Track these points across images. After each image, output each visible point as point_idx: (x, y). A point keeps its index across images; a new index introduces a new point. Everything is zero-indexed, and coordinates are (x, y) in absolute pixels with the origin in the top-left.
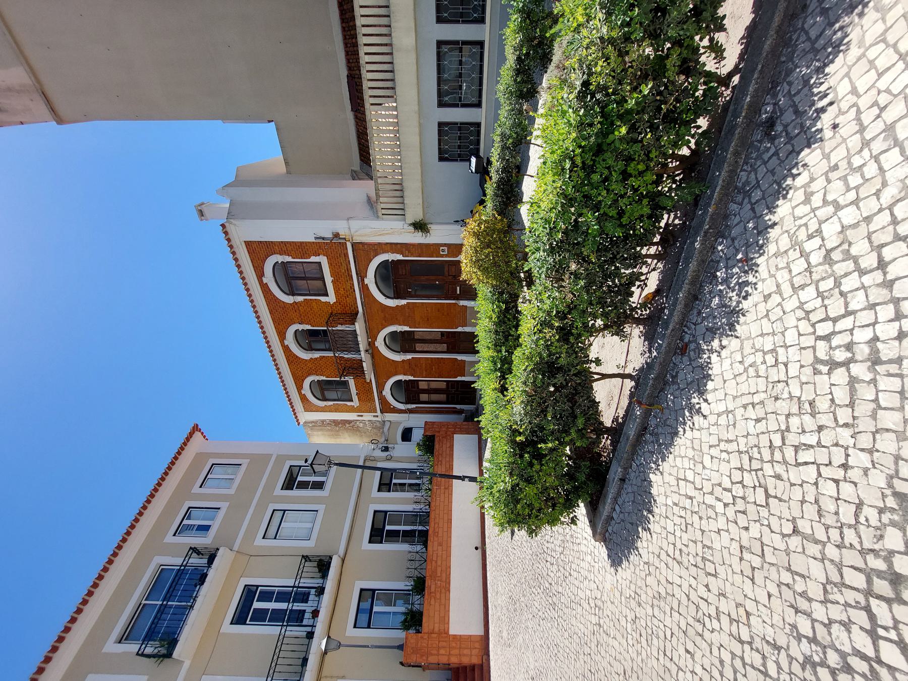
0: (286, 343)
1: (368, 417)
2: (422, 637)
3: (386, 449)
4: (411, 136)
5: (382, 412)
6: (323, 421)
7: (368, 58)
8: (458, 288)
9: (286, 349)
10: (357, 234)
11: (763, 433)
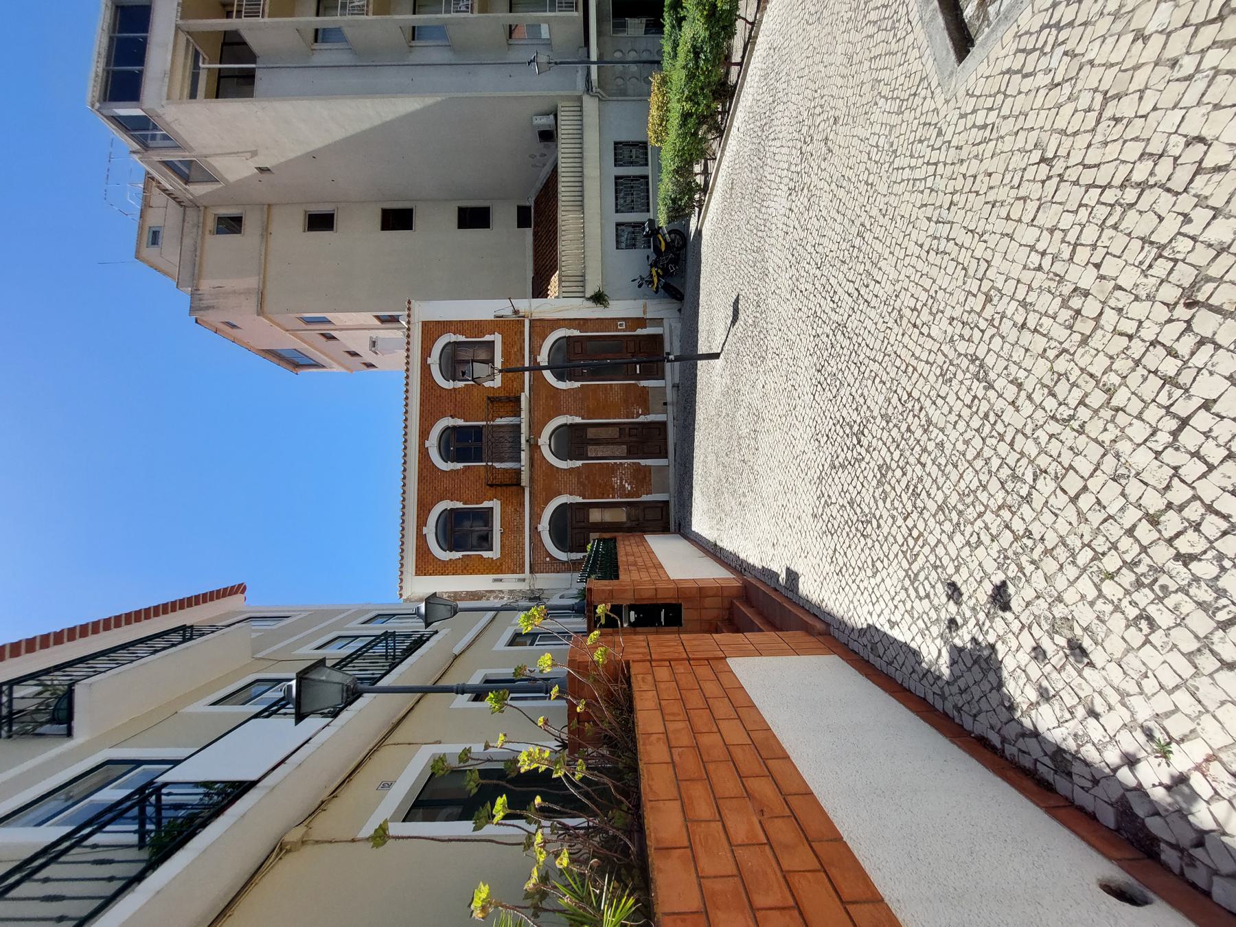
1: (510, 583)
5: (531, 572)
7: (563, 189)
11: (1055, 523)
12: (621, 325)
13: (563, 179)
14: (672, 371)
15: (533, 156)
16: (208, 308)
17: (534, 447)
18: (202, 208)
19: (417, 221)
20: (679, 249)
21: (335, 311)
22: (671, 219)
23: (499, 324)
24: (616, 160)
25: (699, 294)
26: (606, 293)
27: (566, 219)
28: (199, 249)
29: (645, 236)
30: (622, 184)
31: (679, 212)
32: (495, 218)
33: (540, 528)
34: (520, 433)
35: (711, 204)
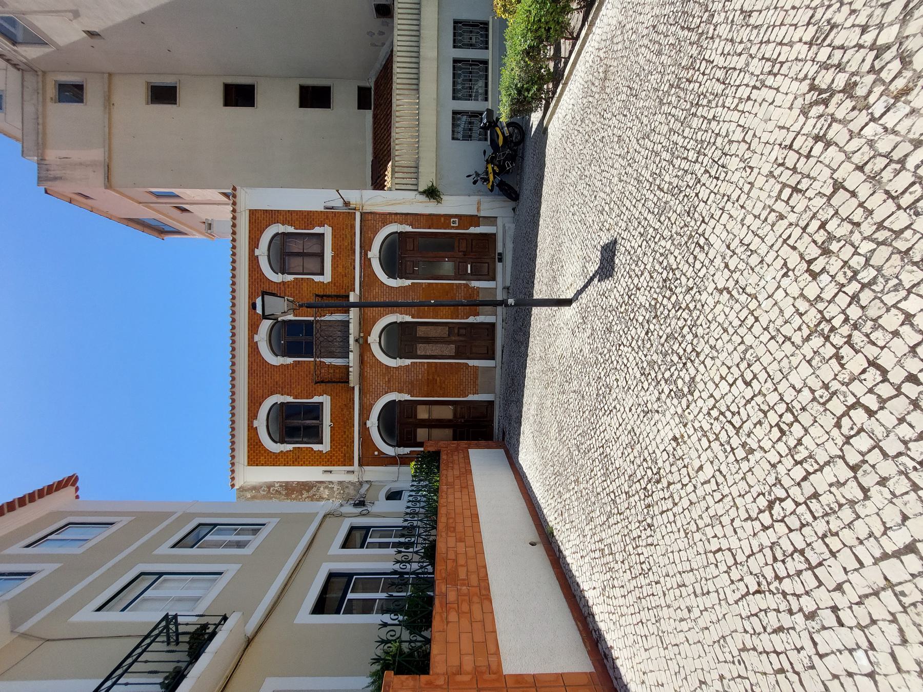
0: (256, 338)
1: (339, 474)
2: (429, 683)
3: (361, 504)
4: (429, 117)
5: (360, 465)
6: (270, 486)
7: (398, 70)
8: (469, 266)
9: (253, 348)
10: (367, 203)
12: (454, 222)
13: (399, 59)
14: (504, 272)
15: (371, 34)
16: (55, 179)
17: (364, 346)
18: (40, 73)
19: (259, 97)
20: (517, 144)
21: (181, 187)
22: (514, 113)
23: (328, 216)
24: (454, 41)
25: (540, 203)
26: (439, 188)
27: (401, 102)
28: (40, 117)
29: (481, 128)
30: (461, 69)
31: (522, 106)
32: (337, 97)
33: (369, 424)
34: (349, 334)
35: (564, 97)
